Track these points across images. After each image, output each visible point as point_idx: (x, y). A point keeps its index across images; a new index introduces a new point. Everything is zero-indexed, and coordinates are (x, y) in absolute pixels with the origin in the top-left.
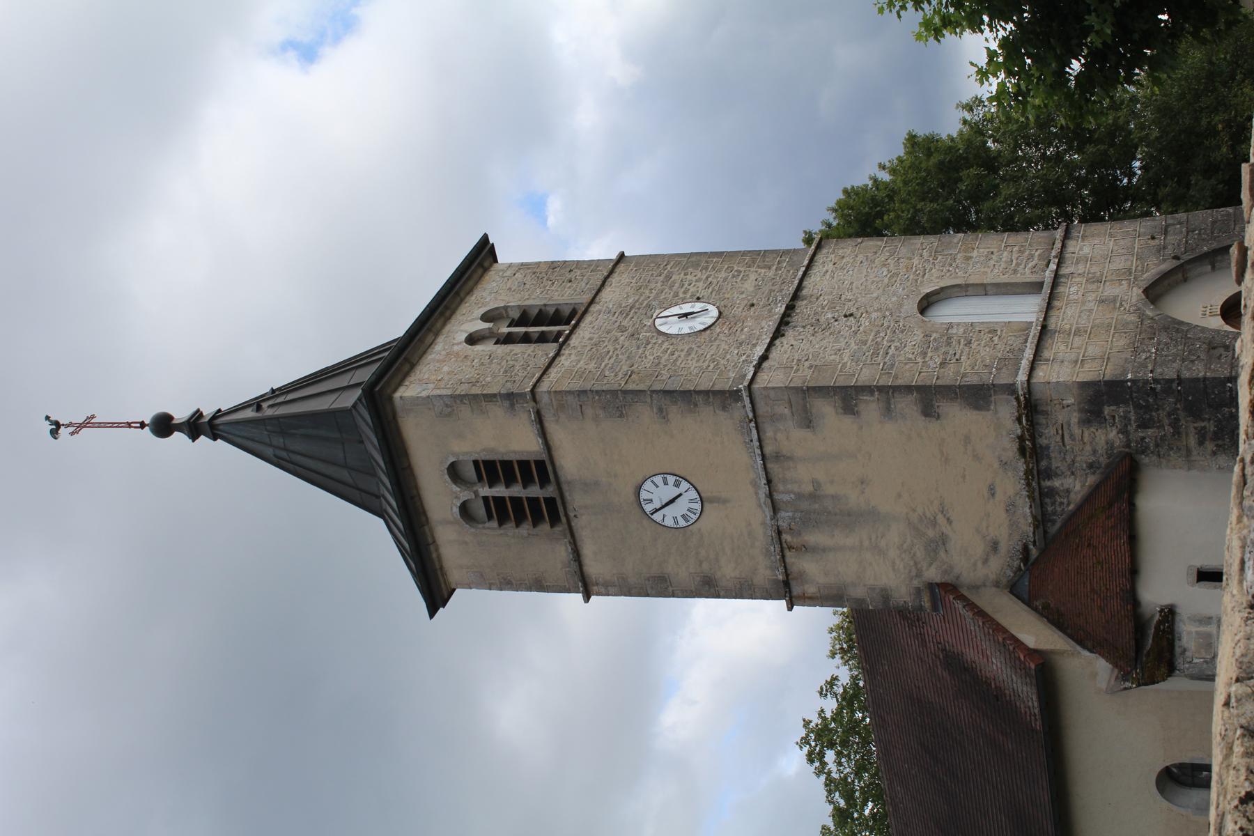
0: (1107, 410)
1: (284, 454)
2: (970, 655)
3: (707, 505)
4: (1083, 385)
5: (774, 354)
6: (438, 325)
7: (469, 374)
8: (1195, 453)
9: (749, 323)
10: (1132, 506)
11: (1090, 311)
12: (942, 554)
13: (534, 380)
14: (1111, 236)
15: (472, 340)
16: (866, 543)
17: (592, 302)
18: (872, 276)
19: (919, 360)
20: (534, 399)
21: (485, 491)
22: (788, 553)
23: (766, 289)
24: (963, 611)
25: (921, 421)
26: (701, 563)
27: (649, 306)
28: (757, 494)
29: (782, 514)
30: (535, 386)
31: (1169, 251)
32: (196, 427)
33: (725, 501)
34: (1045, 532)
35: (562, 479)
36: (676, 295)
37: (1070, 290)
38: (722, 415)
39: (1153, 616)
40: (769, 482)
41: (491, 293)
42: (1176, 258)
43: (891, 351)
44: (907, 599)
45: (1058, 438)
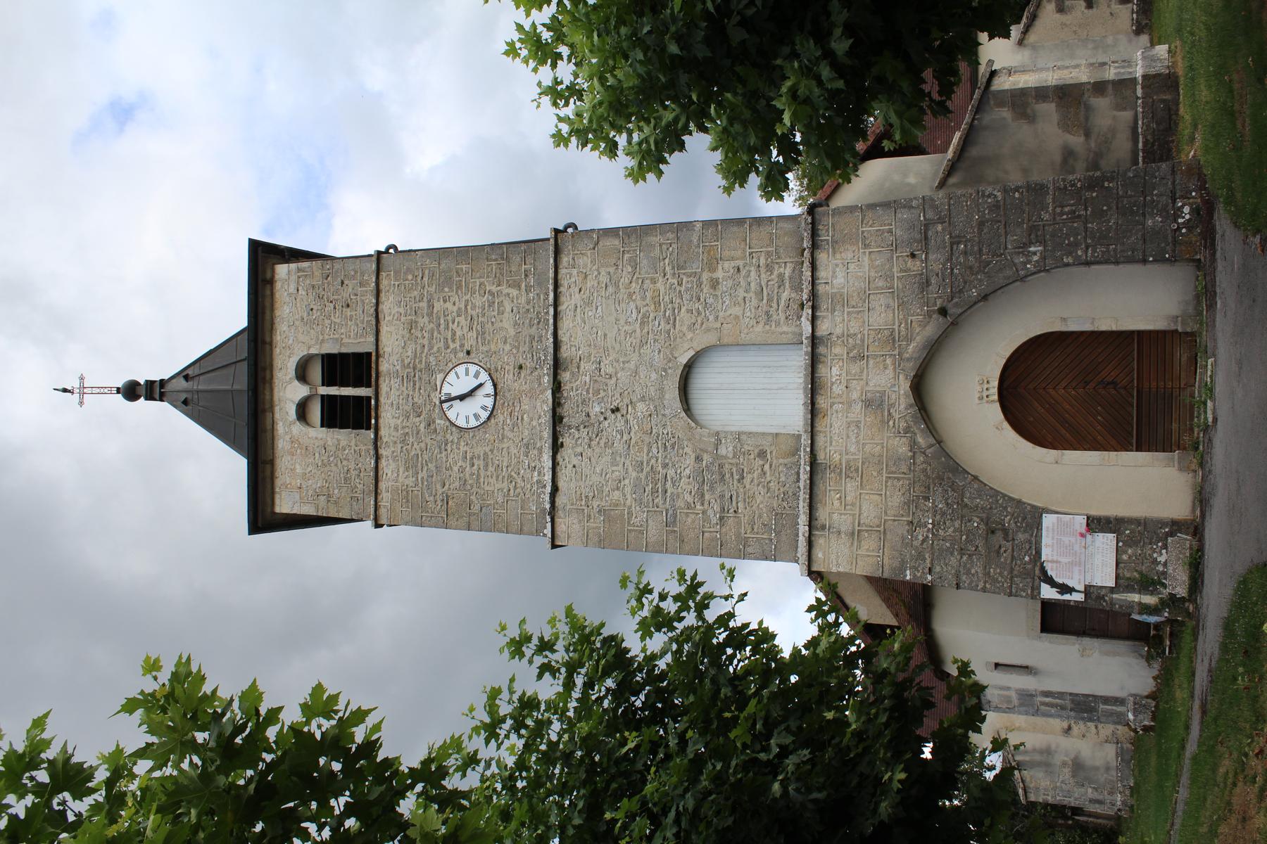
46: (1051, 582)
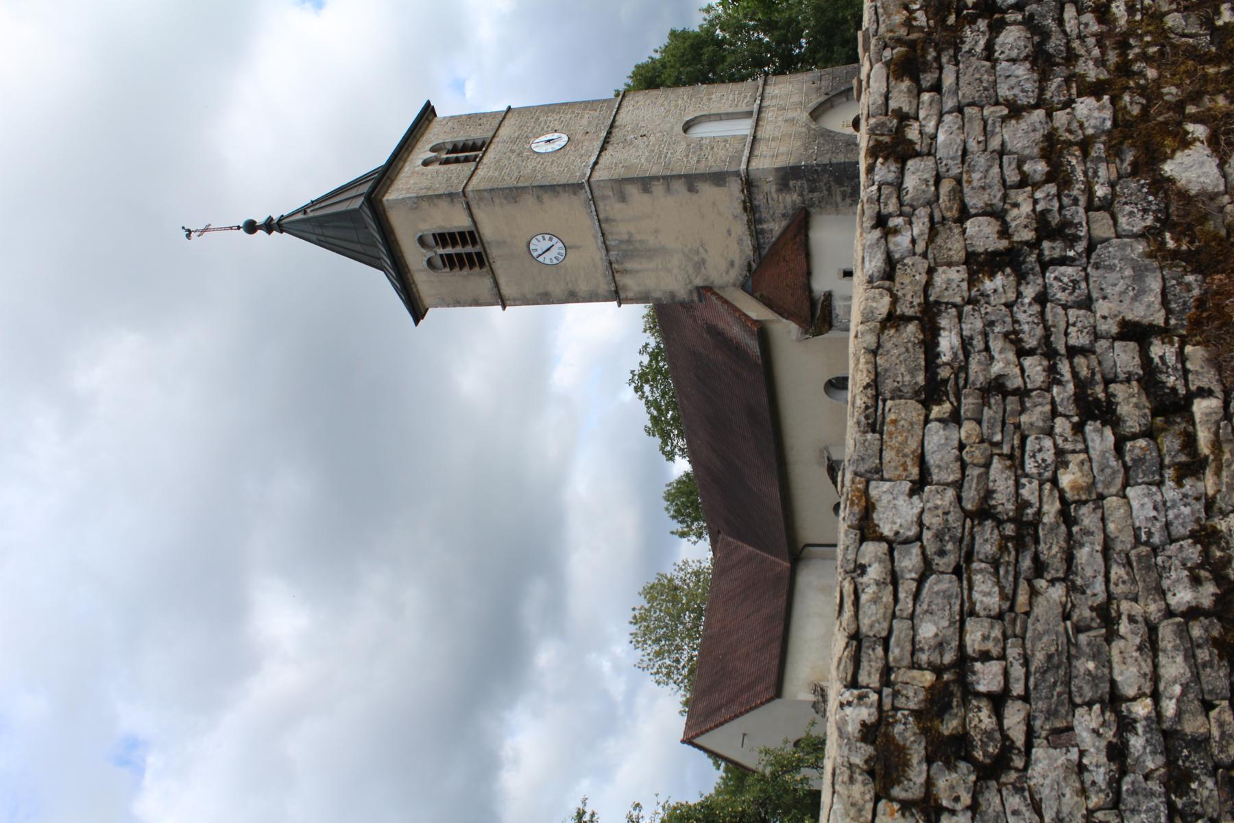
0: (791, 183)
2: (721, 325)
4: (777, 170)
5: (601, 161)
7: (426, 183)
9: (586, 143)
10: (807, 236)
15: (426, 163)
17: (494, 136)
21: (441, 251)
23: (594, 123)
25: (688, 195)
31: (823, 90)
32: (269, 226)
37: (768, 115)
40: (603, 235)
41: (434, 135)
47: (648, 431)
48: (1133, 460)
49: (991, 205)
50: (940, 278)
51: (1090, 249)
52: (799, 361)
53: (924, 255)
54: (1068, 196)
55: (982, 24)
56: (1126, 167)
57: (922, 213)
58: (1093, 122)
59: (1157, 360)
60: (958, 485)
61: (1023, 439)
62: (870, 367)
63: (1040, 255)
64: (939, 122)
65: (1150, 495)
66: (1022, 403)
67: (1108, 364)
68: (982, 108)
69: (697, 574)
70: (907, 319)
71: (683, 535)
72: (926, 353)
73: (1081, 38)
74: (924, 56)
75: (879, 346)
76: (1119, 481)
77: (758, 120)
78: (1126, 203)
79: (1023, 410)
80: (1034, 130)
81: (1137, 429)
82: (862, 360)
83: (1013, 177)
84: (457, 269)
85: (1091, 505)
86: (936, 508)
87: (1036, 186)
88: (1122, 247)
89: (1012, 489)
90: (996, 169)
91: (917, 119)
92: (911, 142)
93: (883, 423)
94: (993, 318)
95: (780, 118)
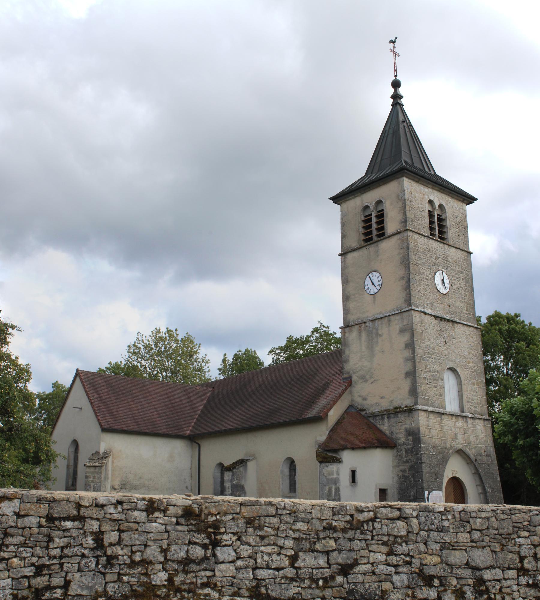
0: (410, 438)
1: (386, 135)
2: (328, 392)
3: (372, 296)
4: (418, 429)
5: (427, 317)
6: (436, 188)
7: (415, 204)
8: (398, 469)
9: (441, 306)
10: (376, 447)
11: (451, 430)
12: (361, 381)
13: (412, 229)
14: (486, 436)
15: (431, 202)
16: (363, 354)
17: (449, 245)
18: (464, 349)
19: (427, 370)
20: (405, 230)
21: (374, 215)
22: (358, 326)
23: (457, 310)
24: (341, 389)
25: (404, 372)
26: (354, 295)
27: (448, 267)
28: (377, 314)
29: (371, 323)
30: (410, 230)
31: (479, 458)
32: (396, 97)
33: (374, 303)
34: (370, 417)
35: (379, 243)
36: (453, 277)
37: (460, 423)
38: (403, 300)
39: (339, 455)
40: (381, 318)
41: (451, 205)
42: (476, 460)
43: (430, 359)
44: (346, 369)
45: (401, 421)
46: (429, 495)
47: (290, 338)
48: (20, 581)
49: (123, 541)
50: (93, 522)
51: (101, 572)
52: (302, 443)
53: (104, 517)
54: (124, 567)
55: (207, 541)
56: (135, 588)
57: (123, 517)
58: (155, 578)
59: (55, 591)
60: (16, 527)
61: (32, 548)
62: (62, 499)
63: (101, 556)
64: (162, 524)
65: (8, 585)
66: (44, 547)
67: (56, 575)
68: (168, 539)
69: (200, 369)
70: (79, 511)
71: (224, 361)
72: (66, 517)
73: (196, 576)
74: (192, 519)
75: (70, 502)
76: (14, 576)
77: (456, 416)
78: (119, 586)
79: (41, 548)
80: (154, 557)
81: (31, 583)
82: (65, 496)
83: (134, 549)
84: (363, 225)
85: (6, 567)
86: (9, 520)
87: (130, 557)
88: (101, 583)
89: (13, 543)
90: (138, 543)
91: (165, 516)
92: (153, 514)
93: (40, 503)
94: (76, 539)
95: (457, 430)
